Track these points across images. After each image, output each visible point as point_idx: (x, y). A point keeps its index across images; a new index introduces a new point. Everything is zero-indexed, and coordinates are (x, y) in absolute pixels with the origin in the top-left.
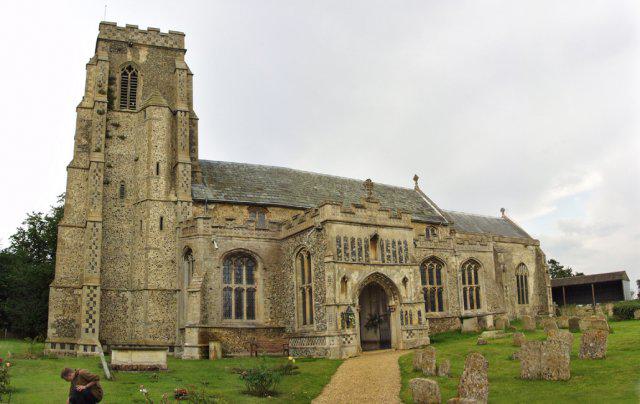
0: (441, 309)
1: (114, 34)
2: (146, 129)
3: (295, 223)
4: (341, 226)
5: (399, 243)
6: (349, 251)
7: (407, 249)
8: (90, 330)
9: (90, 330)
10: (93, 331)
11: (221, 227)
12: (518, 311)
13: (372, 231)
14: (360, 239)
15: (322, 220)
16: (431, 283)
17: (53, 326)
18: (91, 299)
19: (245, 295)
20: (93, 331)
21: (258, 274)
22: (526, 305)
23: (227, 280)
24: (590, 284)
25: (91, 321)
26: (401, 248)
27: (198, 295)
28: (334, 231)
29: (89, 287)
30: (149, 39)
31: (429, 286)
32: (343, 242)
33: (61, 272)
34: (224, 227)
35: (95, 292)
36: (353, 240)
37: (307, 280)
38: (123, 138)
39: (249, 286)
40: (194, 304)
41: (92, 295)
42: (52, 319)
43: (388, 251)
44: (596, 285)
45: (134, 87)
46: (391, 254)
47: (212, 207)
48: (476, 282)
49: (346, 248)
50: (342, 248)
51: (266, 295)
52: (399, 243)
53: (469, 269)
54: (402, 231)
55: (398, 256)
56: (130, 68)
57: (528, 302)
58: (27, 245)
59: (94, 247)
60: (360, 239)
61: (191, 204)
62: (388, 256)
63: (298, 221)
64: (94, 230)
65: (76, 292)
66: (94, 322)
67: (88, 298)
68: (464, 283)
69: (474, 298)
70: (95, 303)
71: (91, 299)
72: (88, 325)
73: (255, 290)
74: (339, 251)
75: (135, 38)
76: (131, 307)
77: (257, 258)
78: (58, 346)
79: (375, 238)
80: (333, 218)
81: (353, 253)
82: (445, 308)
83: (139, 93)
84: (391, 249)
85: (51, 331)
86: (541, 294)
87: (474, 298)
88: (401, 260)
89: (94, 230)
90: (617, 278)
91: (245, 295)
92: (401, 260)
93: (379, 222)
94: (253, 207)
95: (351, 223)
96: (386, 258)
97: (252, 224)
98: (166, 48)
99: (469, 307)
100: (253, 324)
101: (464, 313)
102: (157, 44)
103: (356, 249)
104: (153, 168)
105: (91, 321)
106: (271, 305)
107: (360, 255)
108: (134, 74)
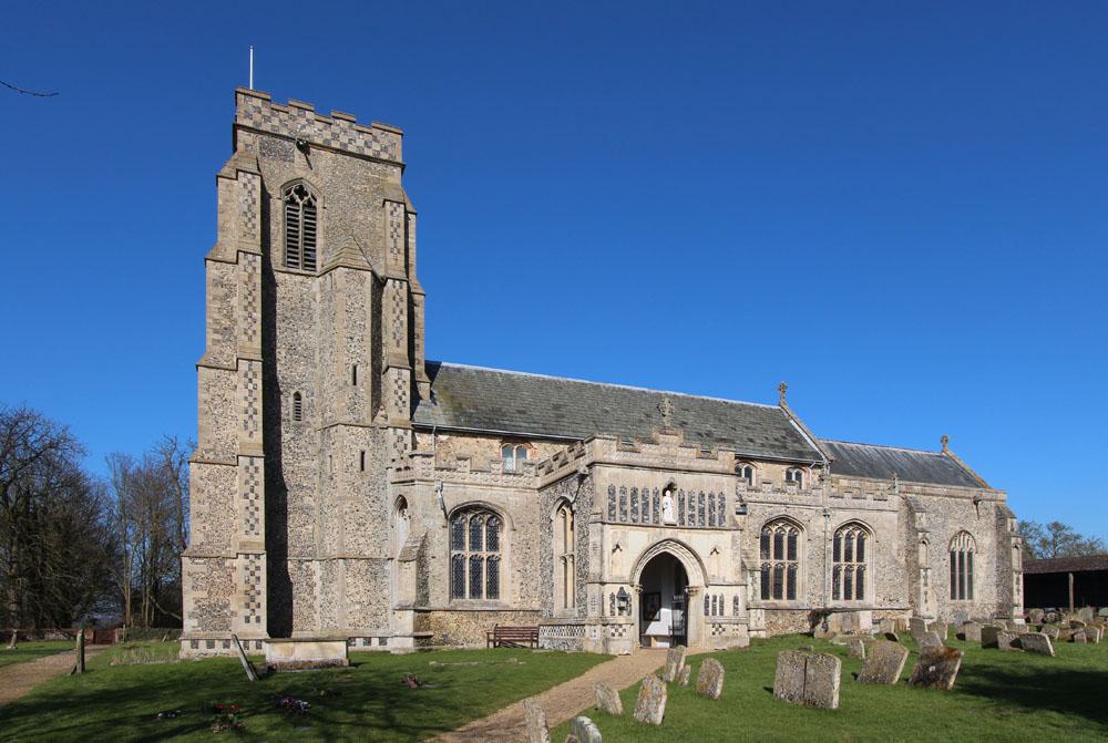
0: (791, 595)
1: (267, 119)
3: (556, 465)
4: (619, 470)
5: (711, 496)
6: (628, 507)
7: (722, 506)
8: (253, 618)
9: (253, 618)
10: (258, 619)
11: (449, 470)
12: (948, 610)
14: (646, 491)
15: (588, 461)
17: (192, 615)
19: (484, 564)
20: (258, 619)
21: (504, 537)
22: (966, 601)
23: (457, 542)
25: (253, 605)
26: (713, 503)
27: (413, 565)
28: (604, 477)
29: (247, 556)
30: (335, 137)
31: (773, 562)
32: (618, 495)
33: (196, 538)
34: (455, 470)
35: (258, 563)
36: (635, 491)
37: (842, 574)
38: (401, 411)
39: (490, 554)
40: (402, 583)
41: (252, 568)
42: (189, 605)
43: (692, 507)
45: (311, 229)
46: (696, 513)
47: (443, 438)
48: (860, 557)
49: (623, 503)
50: (617, 503)
51: (514, 566)
52: (711, 496)
53: (849, 537)
54: (717, 478)
55: (707, 515)
56: (301, 192)
57: (971, 597)
59: (252, 496)
60: (646, 491)
62: (692, 516)
63: (558, 462)
64: (252, 469)
65: (227, 563)
68: (837, 558)
69: (854, 582)
70: (258, 578)
71: (252, 574)
74: (612, 508)
75: (307, 131)
76: (319, 584)
77: (505, 516)
78: (203, 644)
79: (670, 487)
80: (606, 458)
81: (635, 511)
84: (696, 505)
85: (189, 624)
86: (1004, 575)
87: (854, 582)
88: (712, 520)
89: (252, 469)
91: (484, 564)
92: (712, 520)
93: (679, 464)
95: (632, 466)
96: (686, 518)
97: (497, 466)
98: (368, 158)
99: (854, 595)
100: (496, 605)
101: (831, 604)
102: (351, 148)
103: (639, 505)
105: (253, 605)
106: (522, 580)
107: (645, 513)
108: (309, 205)
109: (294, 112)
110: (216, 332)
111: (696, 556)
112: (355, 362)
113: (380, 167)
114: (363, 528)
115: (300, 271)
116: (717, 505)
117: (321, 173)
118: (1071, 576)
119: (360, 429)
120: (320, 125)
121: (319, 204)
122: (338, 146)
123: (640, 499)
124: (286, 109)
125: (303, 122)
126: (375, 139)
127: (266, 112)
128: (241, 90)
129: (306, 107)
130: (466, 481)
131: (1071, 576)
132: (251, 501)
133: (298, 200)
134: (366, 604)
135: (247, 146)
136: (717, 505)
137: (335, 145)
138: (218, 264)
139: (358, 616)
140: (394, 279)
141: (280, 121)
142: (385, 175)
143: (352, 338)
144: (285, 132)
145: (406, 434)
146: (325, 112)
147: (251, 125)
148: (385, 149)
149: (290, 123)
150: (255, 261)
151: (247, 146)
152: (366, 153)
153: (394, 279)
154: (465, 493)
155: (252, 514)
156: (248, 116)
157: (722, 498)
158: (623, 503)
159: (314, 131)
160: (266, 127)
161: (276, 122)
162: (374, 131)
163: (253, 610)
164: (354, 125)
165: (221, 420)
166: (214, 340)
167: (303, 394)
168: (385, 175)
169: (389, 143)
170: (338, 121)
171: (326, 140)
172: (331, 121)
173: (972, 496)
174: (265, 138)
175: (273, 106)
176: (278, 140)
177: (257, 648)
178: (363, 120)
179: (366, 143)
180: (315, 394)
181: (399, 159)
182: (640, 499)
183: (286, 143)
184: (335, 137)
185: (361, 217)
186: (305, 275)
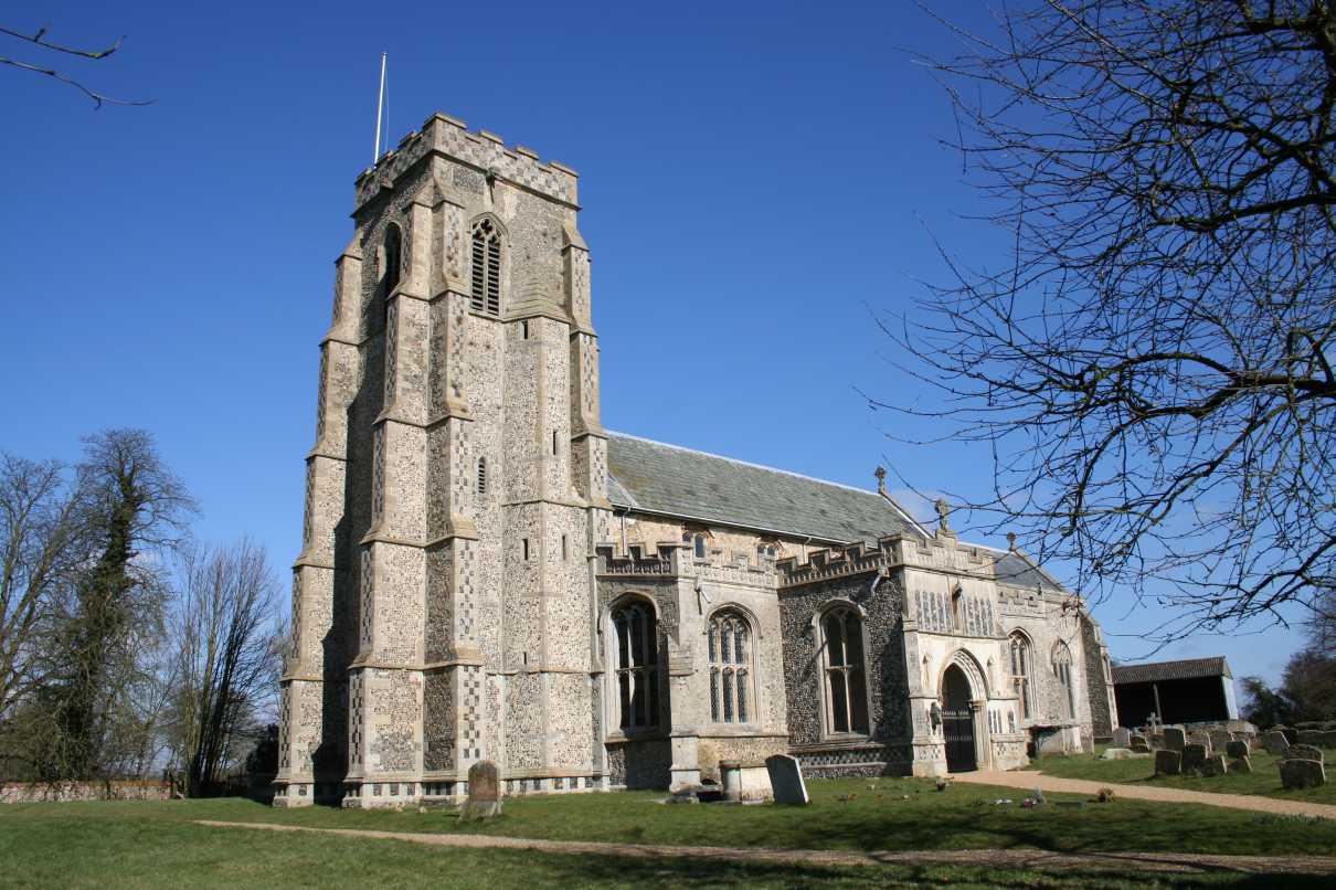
1: (462, 148)
2: (530, 361)
6: (929, 614)
13: (953, 580)
16: (725, 657)
17: (374, 749)
18: (472, 692)
24: (1151, 683)
30: (520, 172)
43: (971, 614)
44: (1162, 684)
49: (926, 610)
50: (922, 610)
56: (487, 227)
58: (1291, 676)
61: (611, 513)
62: (972, 623)
66: (478, 735)
67: (467, 690)
71: (472, 692)
72: (467, 741)
73: (746, 673)
78: (386, 788)
82: (1031, 712)
83: (505, 282)
90: (1209, 672)
94: (768, 536)
102: (533, 186)
104: (548, 439)
109: (486, 143)
110: (406, 379)
111: (976, 662)
112: (555, 426)
113: (558, 208)
114: (566, 633)
115: (484, 313)
116: (987, 612)
117: (509, 205)
118: (1155, 687)
119: (562, 508)
120: (508, 159)
121: (503, 239)
122: (522, 183)
123: (936, 605)
124: (478, 140)
125: (493, 153)
126: (555, 180)
127: (461, 139)
128: (441, 116)
129: (496, 139)
130: (719, 579)
131: (1155, 687)
132: (466, 596)
133: (484, 235)
134: (570, 732)
135: (442, 173)
136: (987, 612)
137: (520, 180)
138: (411, 300)
139: (564, 748)
140: (585, 334)
141: (473, 151)
142: (563, 217)
143: (553, 399)
144: (476, 163)
145: (607, 516)
146: (513, 152)
147: (447, 152)
148: (563, 190)
149: (481, 154)
150: (463, 302)
151: (442, 173)
152: (546, 192)
153: (585, 334)
154: (719, 594)
155: (467, 612)
156: (445, 142)
157: (988, 601)
158: (926, 610)
159: (503, 165)
160: (460, 156)
161: (469, 151)
162: (552, 169)
163: (473, 741)
164: (537, 163)
165: (408, 490)
166: (403, 389)
167: (489, 460)
168: (563, 217)
169: (564, 184)
170: (523, 157)
171: (512, 175)
172: (516, 155)
173: (1062, 601)
174: (459, 167)
175: (468, 135)
176: (470, 171)
177: (557, 787)
178: (545, 159)
179: (546, 182)
180: (499, 461)
181: (574, 202)
182: (936, 605)
183: (477, 174)
184: (520, 172)
185: (542, 260)
186: (491, 319)
